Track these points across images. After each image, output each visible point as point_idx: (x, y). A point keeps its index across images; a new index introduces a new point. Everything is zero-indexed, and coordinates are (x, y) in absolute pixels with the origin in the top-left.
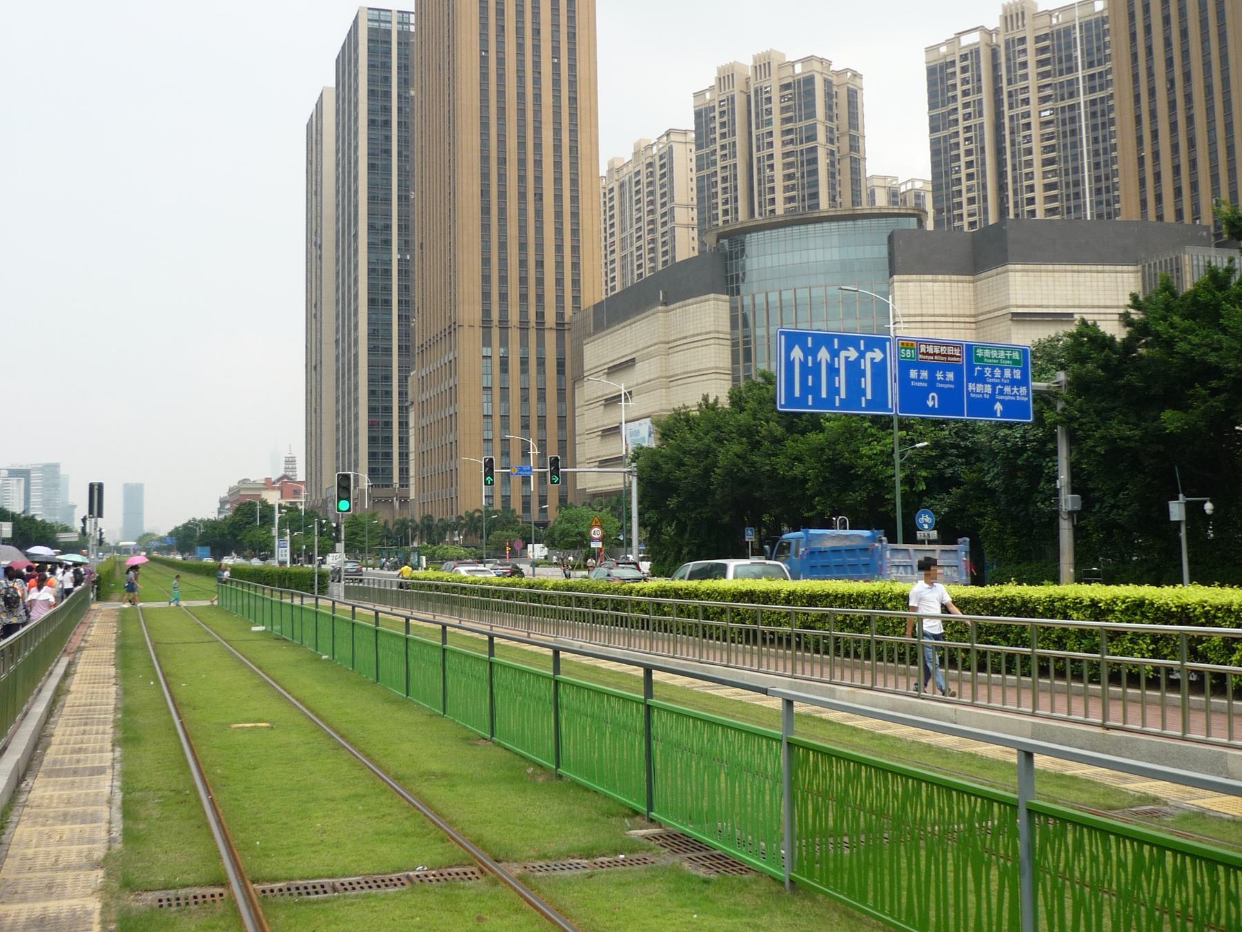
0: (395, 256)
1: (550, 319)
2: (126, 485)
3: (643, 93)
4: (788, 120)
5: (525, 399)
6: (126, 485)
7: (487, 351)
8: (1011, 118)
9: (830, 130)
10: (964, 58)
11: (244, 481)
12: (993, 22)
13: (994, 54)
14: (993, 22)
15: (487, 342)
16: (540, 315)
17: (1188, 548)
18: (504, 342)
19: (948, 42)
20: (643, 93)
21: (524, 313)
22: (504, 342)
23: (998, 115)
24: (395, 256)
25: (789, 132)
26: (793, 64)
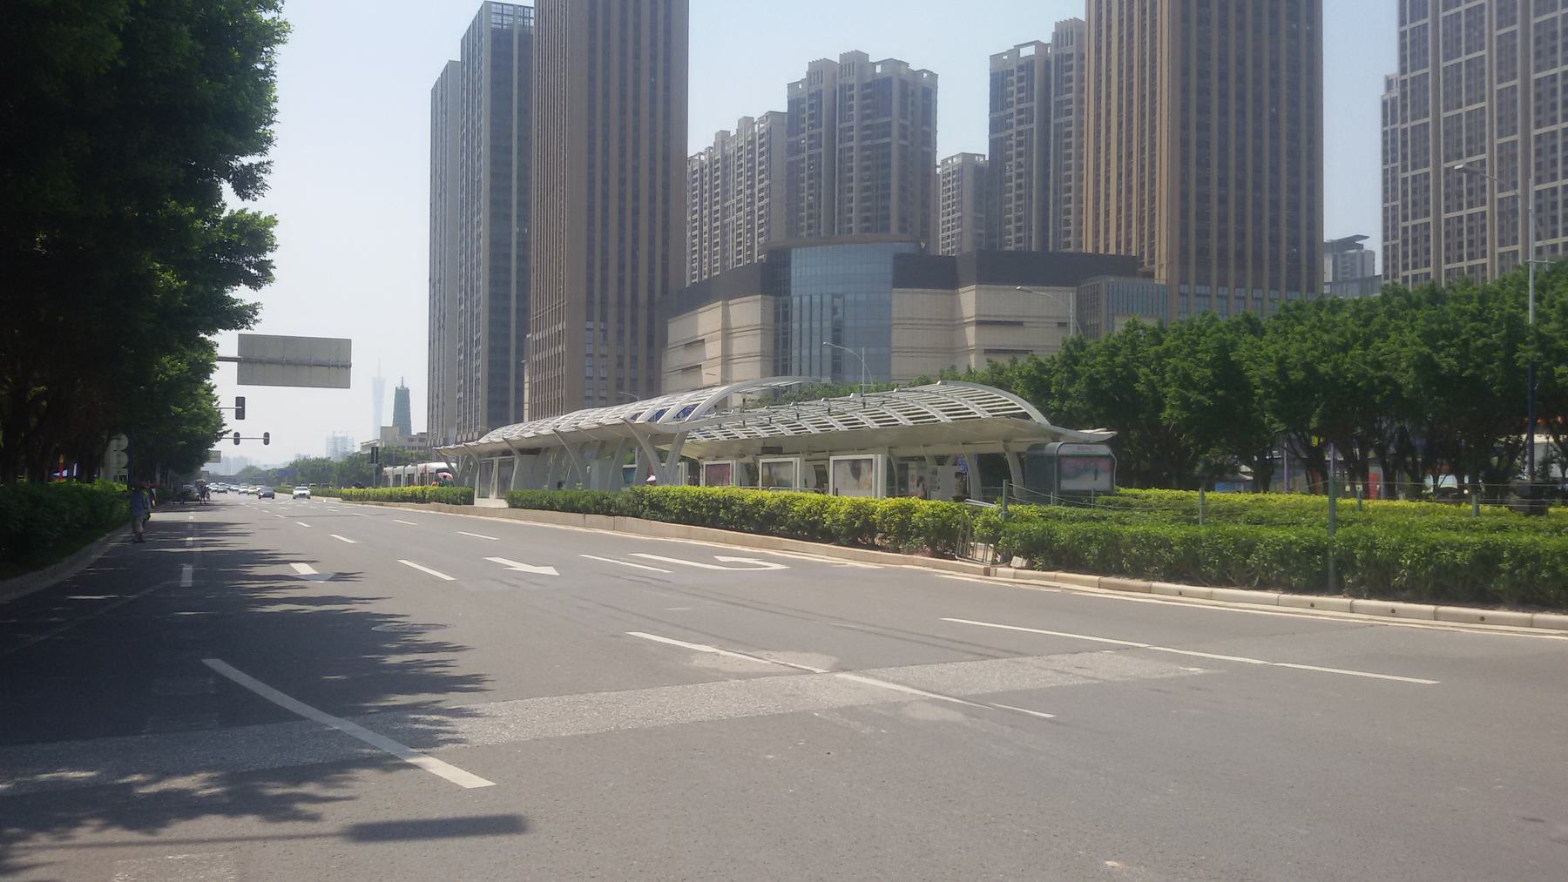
0: (515, 230)
1: (643, 296)
2: (346, 344)
3: (731, 87)
4: (868, 117)
5: (634, 358)
6: (346, 344)
7: (589, 325)
8: (1056, 126)
9: (903, 127)
10: (1021, 68)
11: (818, 70)
12: (1047, 38)
13: (1047, 64)
14: (1047, 38)
15: (590, 318)
16: (634, 297)
17: (255, 675)
18: (604, 319)
19: (1009, 52)
20: (731, 87)
21: (621, 292)
22: (604, 319)
23: (1046, 121)
24: (515, 230)
25: (868, 127)
26: (874, 64)
